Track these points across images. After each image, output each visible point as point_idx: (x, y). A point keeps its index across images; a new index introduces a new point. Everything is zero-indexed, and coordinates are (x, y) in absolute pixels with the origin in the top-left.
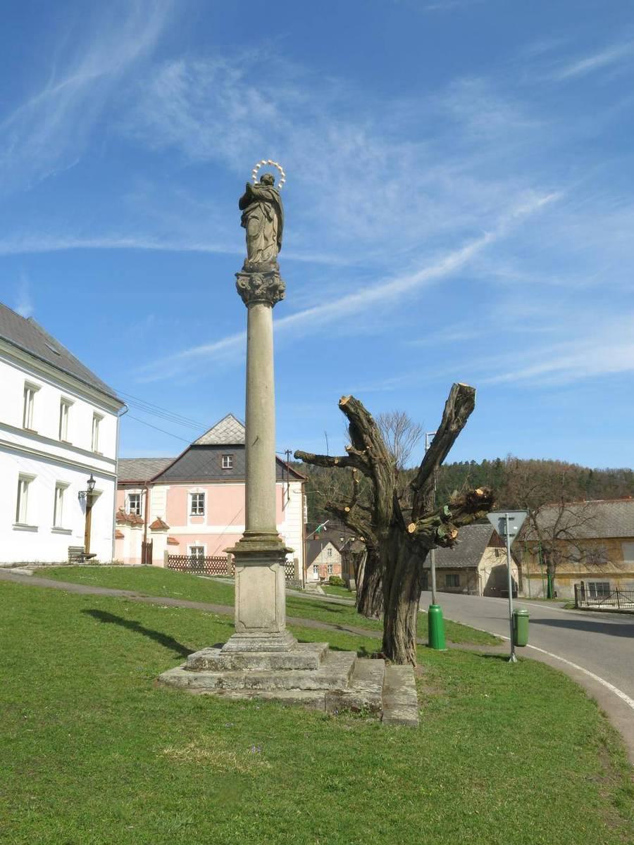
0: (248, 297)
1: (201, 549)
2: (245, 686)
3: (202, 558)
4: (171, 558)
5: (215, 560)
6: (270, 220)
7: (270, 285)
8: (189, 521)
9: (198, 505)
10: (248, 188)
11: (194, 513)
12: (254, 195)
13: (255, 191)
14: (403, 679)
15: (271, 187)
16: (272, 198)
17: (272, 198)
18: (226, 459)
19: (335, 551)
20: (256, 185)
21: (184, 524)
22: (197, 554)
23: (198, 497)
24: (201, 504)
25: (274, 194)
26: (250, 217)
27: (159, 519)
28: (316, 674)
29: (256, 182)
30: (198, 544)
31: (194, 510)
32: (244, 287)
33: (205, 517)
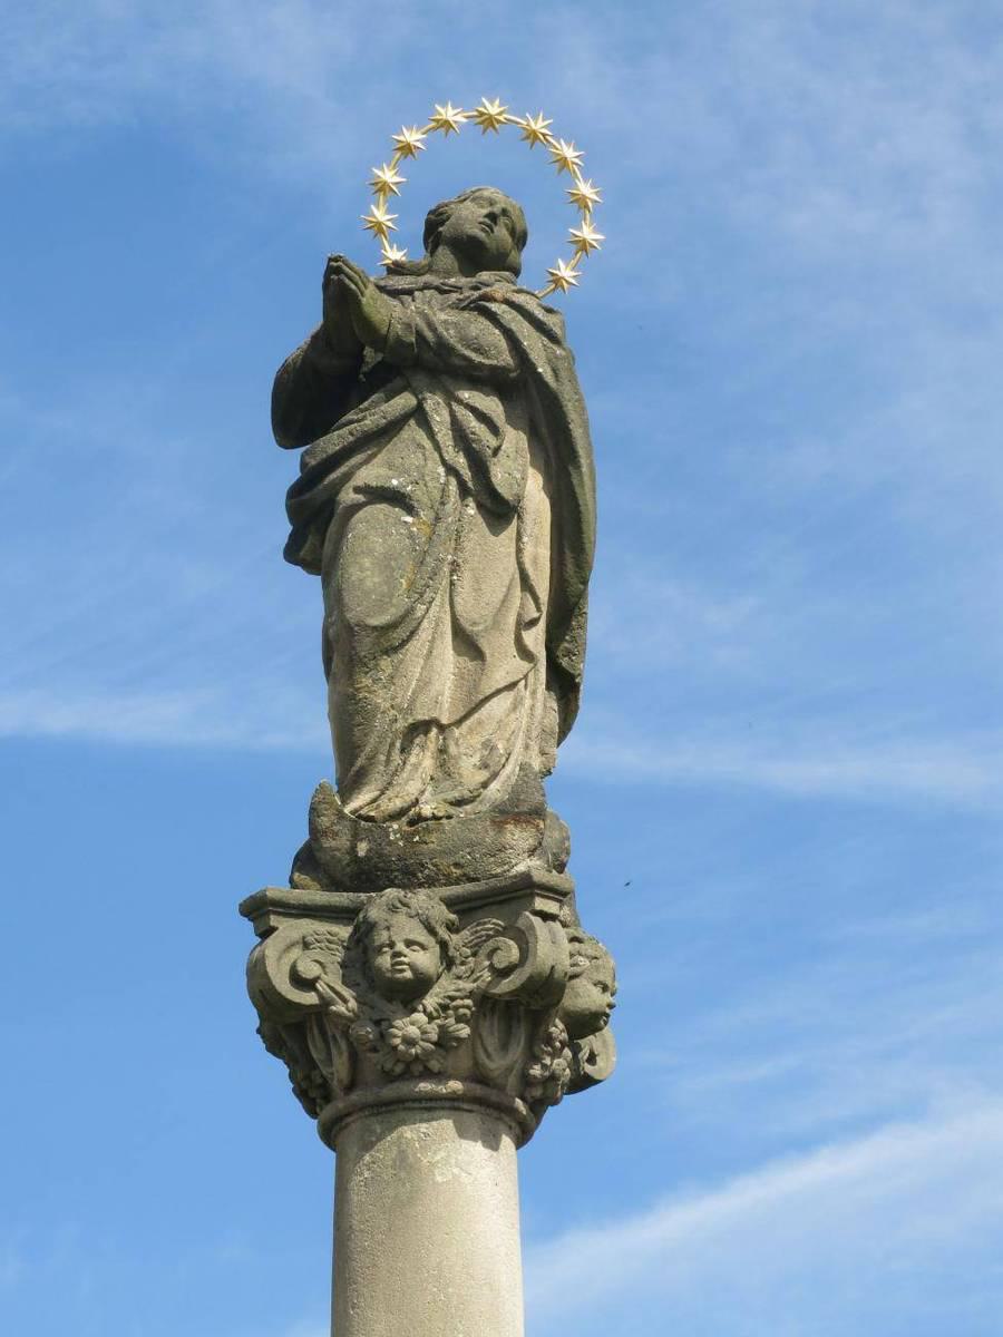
6: (500, 511)
12: (379, 339)
15: (495, 283)
16: (505, 358)
17: (505, 358)
20: (396, 269)
26: (348, 496)
32: (310, 998)
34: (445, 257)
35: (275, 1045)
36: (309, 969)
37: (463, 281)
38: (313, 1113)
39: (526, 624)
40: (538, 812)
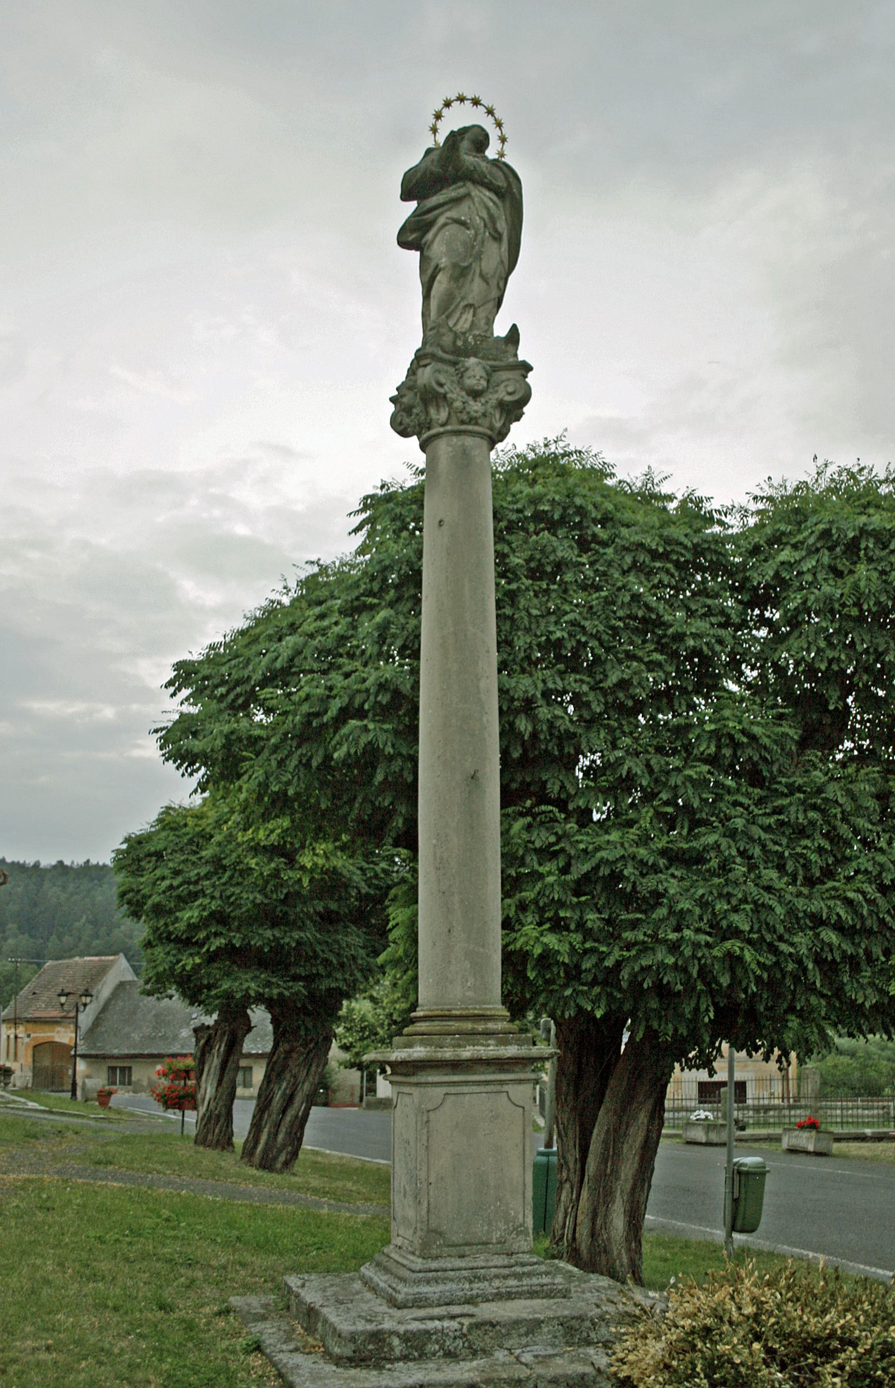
0: (443, 415)
7: (510, 394)
32: (441, 390)
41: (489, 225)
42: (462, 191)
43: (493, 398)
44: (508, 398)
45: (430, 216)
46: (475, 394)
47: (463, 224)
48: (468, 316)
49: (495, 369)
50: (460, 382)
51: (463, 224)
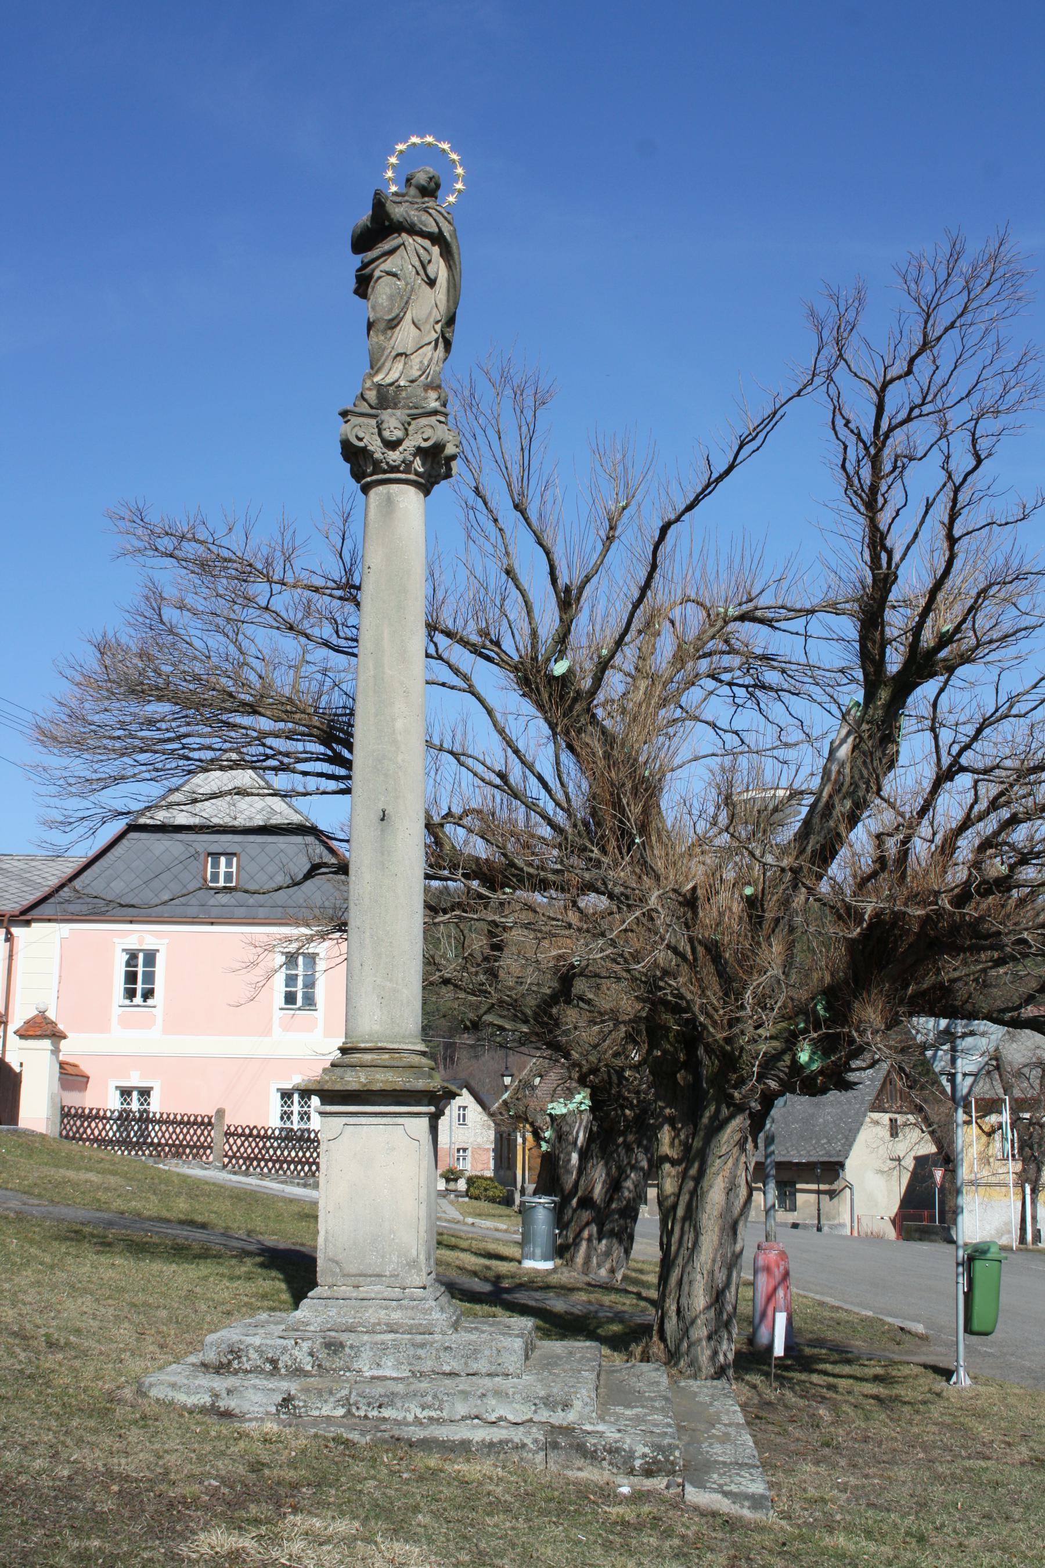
1: (145, 1093)
2: (349, 1411)
3: (145, 1119)
4: (68, 1115)
5: (181, 1122)
6: (432, 283)
7: (425, 440)
8: (114, 1019)
9: (138, 980)
10: (379, 205)
11: (127, 1002)
12: (390, 220)
13: (398, 212)
14: (712, 1410)
15: (430, 202)
16: (436, 230)
17: (436, 230)
18: (216, 865)
19: (474, 1111)
20: (395, 194)
21: (103, 1027)
22: (135, 1106)
23: (141, 956)
24: (149, 977)
25: (440, 219)
26: (377, 273)
27: (42, 1013)
28: (506, 1392)
29: (394, 189)
30: (135, 1080)
31: (131, 994)
32: (361, 444)
33: (158, 1012)
34: (413, 191)
35: (347, 459)
36: (361, 435)
37: (419, 200)
38: (358, 482)
39: (437, 322)
40: (439, 387)
41: (422, 272)
42: (399, 241)
43: (409, 444)
44: (424, 445)
45: (367, 271)
46: (392, 445)
47: (395, 275)
48: (399, 365)
49: (414, 417)
50: (380, 434)
51: (395, 275)
